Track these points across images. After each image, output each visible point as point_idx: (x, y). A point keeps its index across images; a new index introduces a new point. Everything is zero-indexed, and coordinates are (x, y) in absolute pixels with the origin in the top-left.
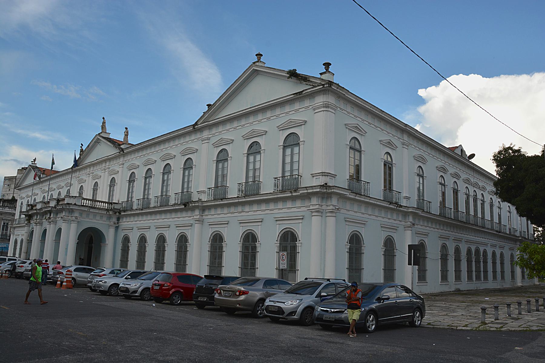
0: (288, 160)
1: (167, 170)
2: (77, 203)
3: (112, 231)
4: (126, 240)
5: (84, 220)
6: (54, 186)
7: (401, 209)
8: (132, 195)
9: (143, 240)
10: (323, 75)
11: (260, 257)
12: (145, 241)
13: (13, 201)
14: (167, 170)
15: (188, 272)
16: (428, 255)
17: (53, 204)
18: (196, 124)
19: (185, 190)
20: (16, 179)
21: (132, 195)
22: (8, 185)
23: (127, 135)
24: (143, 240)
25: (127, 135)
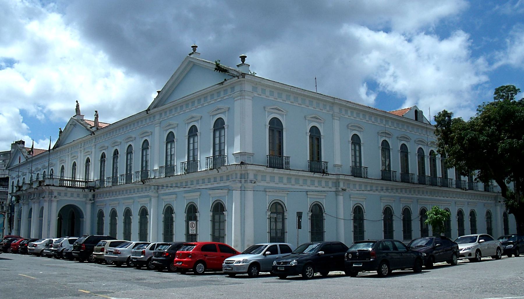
0: (217, 141)
1: (129, 151)
2: (55, 184)
3: (89, 207)
4: (101, 215)
5: (63, 198)
6: (40, 167)
7: (329, 177)
8: (146, 158)
9: (128, 213)
10: (240, 67)
11: (509, 223)
12: (116, 215)
13: (7, 179)
14: (129, 151)
15: (226, 243)
16: (365, 217)
17: (35, 186)
18: (149, 110)
19: (144, 169)
20: (10, 154)
21: (146, 158)
22: (4, 161)
23: (97, 118)
24: (128, 213)
25: (97, 118)
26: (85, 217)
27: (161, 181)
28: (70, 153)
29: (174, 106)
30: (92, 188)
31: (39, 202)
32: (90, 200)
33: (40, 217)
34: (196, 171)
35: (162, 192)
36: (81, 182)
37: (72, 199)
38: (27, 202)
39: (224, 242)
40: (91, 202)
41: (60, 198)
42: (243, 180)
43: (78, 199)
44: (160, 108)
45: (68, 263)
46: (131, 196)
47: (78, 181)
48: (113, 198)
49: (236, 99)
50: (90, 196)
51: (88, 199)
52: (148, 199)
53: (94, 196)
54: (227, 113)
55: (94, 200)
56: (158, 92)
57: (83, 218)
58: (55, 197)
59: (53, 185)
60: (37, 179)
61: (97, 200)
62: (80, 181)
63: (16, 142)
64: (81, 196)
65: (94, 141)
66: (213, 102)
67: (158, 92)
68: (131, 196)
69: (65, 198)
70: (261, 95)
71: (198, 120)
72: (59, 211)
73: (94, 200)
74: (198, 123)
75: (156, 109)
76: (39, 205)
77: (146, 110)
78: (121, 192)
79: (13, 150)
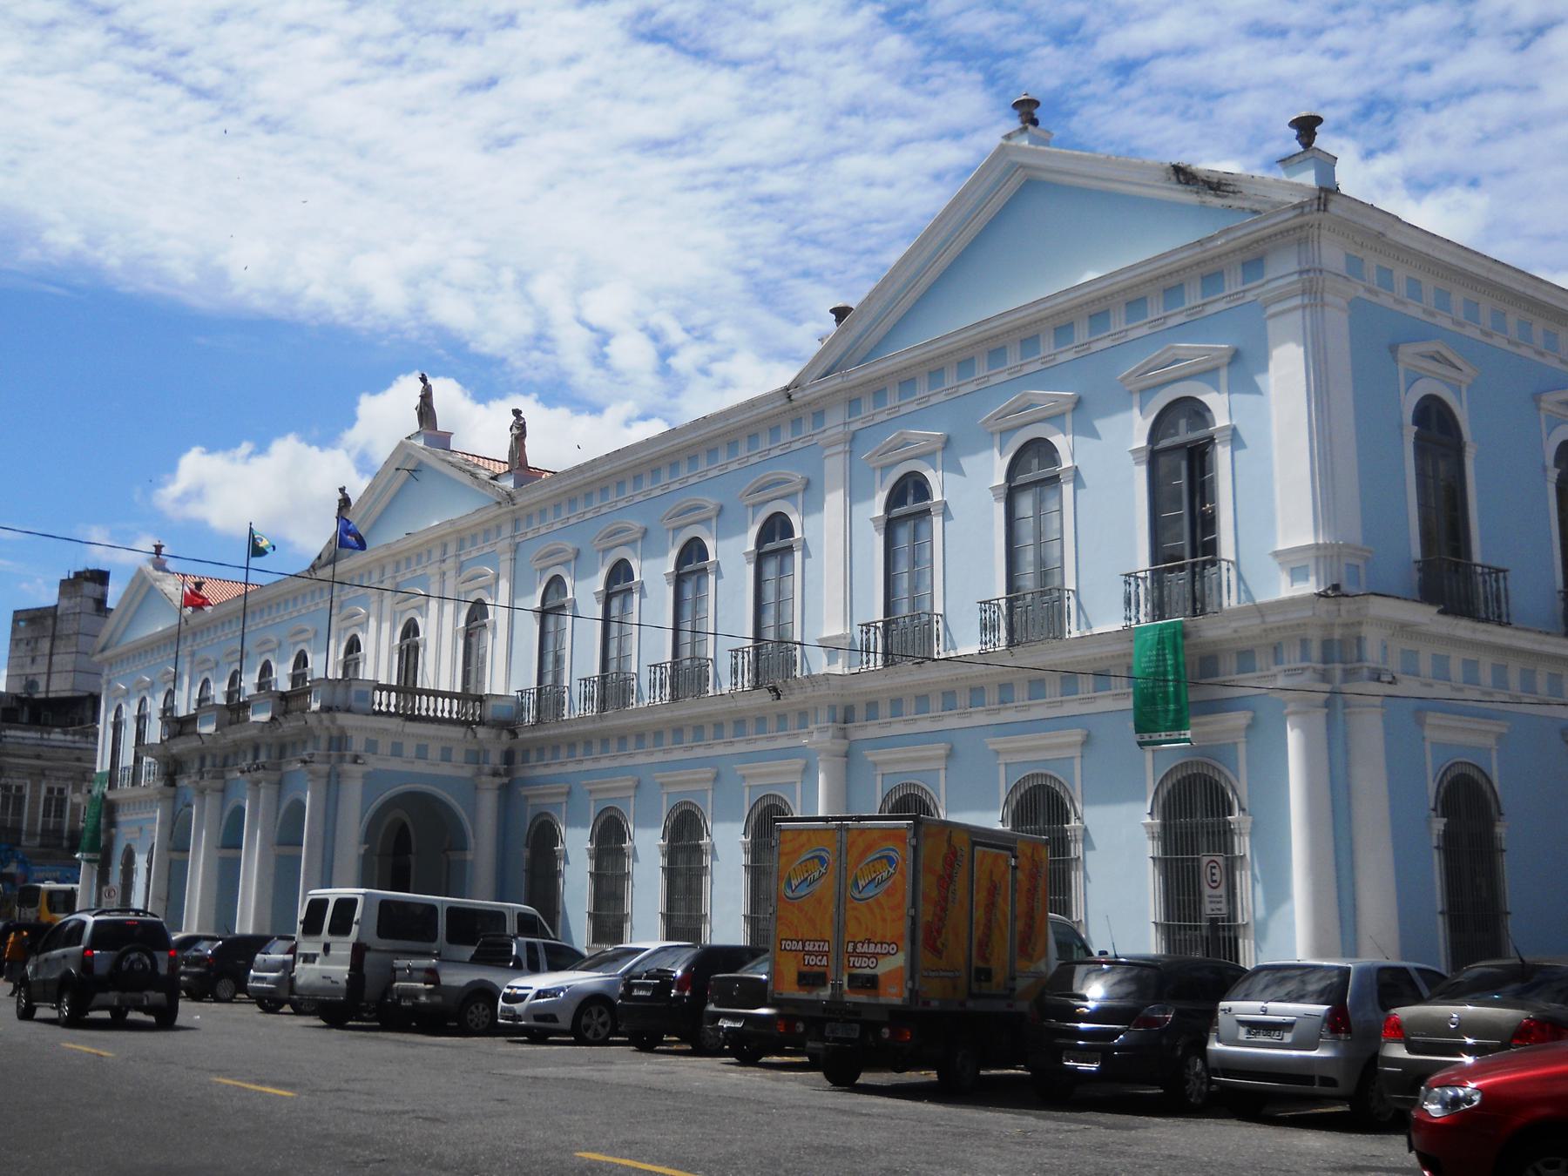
26: (471, 842)
27: (742, 703)
28: (450, 564)
29: (684, 449)
30: (509, 724)
31: (223, 791)
32: (495, 774)
33: (224, 847)
34: (1059, 635)
35: (873, 731)
36: (444, 695)
37: (420, 767)
38: (218, 784)
39: (1237, 960)
40: (498, 781)
41: (374, 763)
42: (1337, 669)
43: (446, 769)
44: (857, 374)
45: (784, 1080)
46: (700, 752)
47: (422, 692)
48: (605, 764)
49: (1273, 309)
50: (495, 759)
51: (487, 768)
52: (798, 764)
53: (509, 757)
54: (800, 496)
55: (508, 773)
56: (840, 313)
57: (464, 848)
58: (355, 759)
59: (348, 710)
60: (262, 685)
61: (524, 772)
62: (436, 694)
63: (77, 574)
64: (458, 755)
65: (507, 530)
66: (884, 417)
67: (840, 313)
68: (700, 752)
69: (395, 765)
70: (1376, 294)
71: (710, 519)
72: (371, 811)
73: (508, 773)
74: (635, 551)
75: (835, 382)
76: (280, 795)
77: (787, 388)
78: (643, 736)
79: (65, 603)
